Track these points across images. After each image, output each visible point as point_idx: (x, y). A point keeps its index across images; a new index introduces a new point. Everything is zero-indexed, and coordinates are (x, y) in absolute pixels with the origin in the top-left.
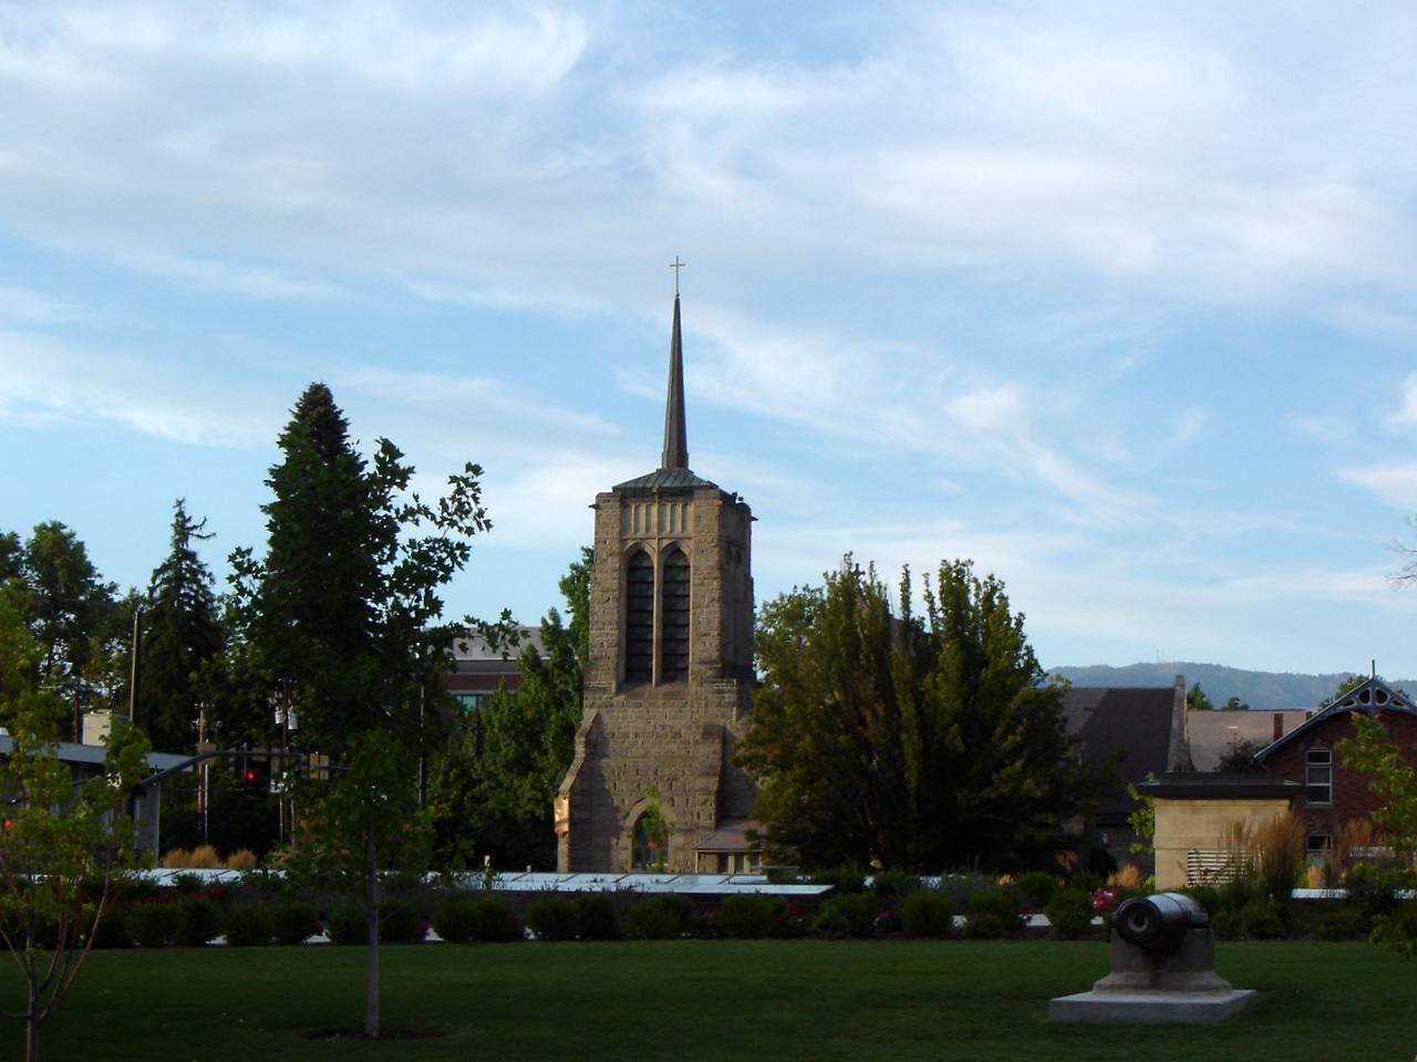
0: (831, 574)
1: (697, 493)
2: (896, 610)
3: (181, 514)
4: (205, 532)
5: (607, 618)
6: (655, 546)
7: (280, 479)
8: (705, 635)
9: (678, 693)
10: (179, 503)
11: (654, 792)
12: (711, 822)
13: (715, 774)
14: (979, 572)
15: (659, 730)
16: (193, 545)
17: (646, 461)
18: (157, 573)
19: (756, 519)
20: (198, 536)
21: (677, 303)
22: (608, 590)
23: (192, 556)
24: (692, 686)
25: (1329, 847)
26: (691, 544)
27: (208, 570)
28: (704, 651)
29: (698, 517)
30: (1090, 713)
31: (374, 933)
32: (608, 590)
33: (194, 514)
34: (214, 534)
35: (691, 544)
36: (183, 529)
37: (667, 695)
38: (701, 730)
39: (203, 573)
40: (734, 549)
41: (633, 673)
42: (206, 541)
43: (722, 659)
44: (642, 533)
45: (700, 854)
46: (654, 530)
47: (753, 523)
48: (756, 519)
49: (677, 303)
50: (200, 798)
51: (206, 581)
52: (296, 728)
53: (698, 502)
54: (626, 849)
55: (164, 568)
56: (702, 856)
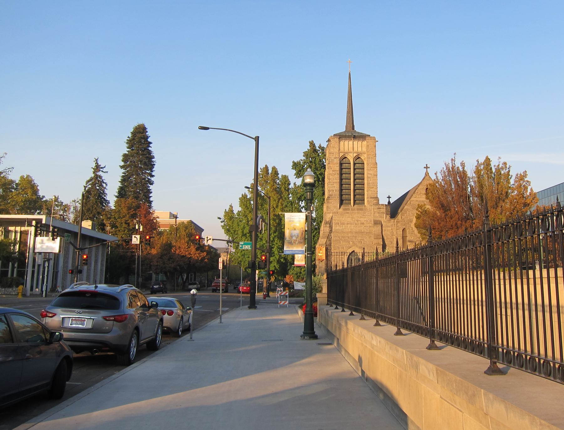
0: (464, 162)
3: (97, 163)
4: (104, 170)
5: (335, 181)
7: (126, 158)
8: (372, 188)
10: (97, 160)
11: (354, 244)
12: (296, 256)
16: (100, 173)
17: (342, 128)
18: (88, 181)
20: (102, 171)
21: (350, 74)
22: (335, 171)
23: (100, 177)
25: (537, 264)
26: (366, 156)
27: (105, 181)
29: (368, 146)
31: (33, 269)
32: (335, 171)
34: (107, 172)
35: (366, 156)
36: (98, 168)
39: (104, 183)
42: (103, 173)
44: (346, 150)
49: (350, 74)
50: (28, 251)
51: (104, 185)
53: (367, 140)
55: (91, 180)
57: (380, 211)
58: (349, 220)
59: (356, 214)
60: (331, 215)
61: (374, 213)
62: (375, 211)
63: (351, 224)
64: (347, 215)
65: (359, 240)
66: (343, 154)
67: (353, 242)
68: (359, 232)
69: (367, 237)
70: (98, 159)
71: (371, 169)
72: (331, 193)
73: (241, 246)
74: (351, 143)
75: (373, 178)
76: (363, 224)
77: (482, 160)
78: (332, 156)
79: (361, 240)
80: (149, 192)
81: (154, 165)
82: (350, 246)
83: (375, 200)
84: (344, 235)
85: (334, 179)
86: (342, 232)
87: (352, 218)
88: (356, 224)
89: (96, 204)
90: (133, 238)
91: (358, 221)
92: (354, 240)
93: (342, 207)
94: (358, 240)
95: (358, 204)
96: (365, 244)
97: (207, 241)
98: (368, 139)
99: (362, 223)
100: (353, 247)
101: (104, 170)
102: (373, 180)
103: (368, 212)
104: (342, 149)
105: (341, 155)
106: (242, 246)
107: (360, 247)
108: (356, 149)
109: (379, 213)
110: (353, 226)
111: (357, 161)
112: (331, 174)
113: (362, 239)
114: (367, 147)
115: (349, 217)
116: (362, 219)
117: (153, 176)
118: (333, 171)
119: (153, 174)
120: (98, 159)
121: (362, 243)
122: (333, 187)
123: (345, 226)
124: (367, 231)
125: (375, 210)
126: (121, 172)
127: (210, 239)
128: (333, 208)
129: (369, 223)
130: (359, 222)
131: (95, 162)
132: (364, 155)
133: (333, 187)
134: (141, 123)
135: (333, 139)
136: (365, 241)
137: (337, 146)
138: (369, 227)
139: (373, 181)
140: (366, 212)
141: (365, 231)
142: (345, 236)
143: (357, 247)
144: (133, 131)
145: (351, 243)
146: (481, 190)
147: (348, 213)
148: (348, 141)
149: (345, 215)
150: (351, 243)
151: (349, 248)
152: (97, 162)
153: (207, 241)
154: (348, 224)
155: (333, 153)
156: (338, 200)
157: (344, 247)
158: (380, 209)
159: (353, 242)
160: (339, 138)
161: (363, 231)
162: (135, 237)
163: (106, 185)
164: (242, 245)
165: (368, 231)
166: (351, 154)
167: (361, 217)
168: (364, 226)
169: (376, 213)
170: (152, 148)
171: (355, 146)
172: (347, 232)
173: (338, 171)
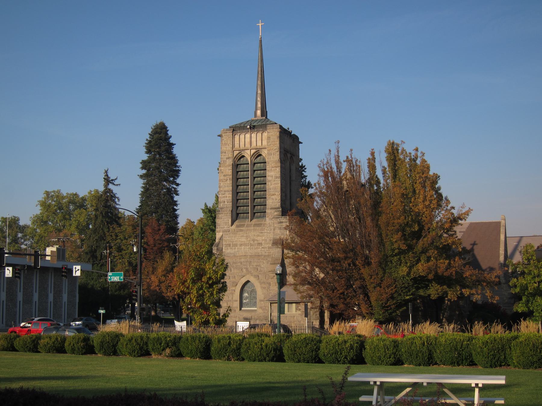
1: (269, 127)
2: (364, 178)
3: (107, 175)
4: (116, 183)
5: (226, 189)
6: (249, 153)
7: (145, 165)
8: (273, 195)
9: (261, 224)
10: (106, 172)
11: (248, 272)
13: (278, 264)
14: (409, 148)
15: (252, 242)
16: (111, 186)
19: (302, 143)
24: (268, 220)
28: (272, 203)
29: (269, 138)
30: (462, 233)
32: (227, 175)
33: (112, 176)
34: (120, 185)
37: (255, 225)
38: (272, 242)
39: (115, 197)
40: (289, 155)
41: (236, 216)
43: (282, 206)
44: (242, 146)
45: (271, 303)
46: (248, 145)
47: (300, 145)
48: (302, 143)
51: (116, 200)
52: (281, 272)
54: (237, 301)
56: (272, 304)
57: (282, 227)
58: (243, 239)
59: (251, 231)
60: (221, 234)
61: (274, 229)
62: (275, 227)
63: (245, 245)
64: (241, 233)
65: (255, 266)
66: (238, 152)
67: (247, 269)
68: (256, 255)
69: (264, 261)
70: (107, 170)
71: (273, 169)
72: (222, 205)
73: (109, 277)
74: (248, 136)
75: (274, 181)
76: (260, 244)
77: (104, 180)
78: (224, 156)
79: (256, 266)
80: (175, 203)
81: (180, 170)
82: (243, 274)
83: (275, 211)
84: (236, 260)
85: (225, 186)
86: (235, 256)
87: (247, 237)
88: (251, 245)
89: (103, 224)
90: (7, 271)
91: (254, 240)
92: (248, 267)
93: (236, 223)
94: (252, 266)
95: (257, 218)
96: (261, 271)
97: (76, 272)
98: (269, 129)
99: (259, 244)
100: (248, 276)
101: (116, 183)
102: (274, 184)
103: (267, 227)
104: (237, 146)
105: (236, 153)
106: (111, 278)
107: (255, 276)
108: (254, 144)
109: (280, 229)
110: (248, 247)
111: (258, 160)
112: (222, 180)
113: (258, 264)
114: (268, 139)
115: (242, 236)
116: (259, 238)
117: (178, 185)
118: (224, 176)
119: (178, 181)
120: (107, 170)
121: (257, 269)
122: (224, 197)
123: (238, 248)
124: (265, 254)
125: (276, 226)
126: (140, 183)
127: (78, 270)
128: (223, 225)
129: (267, 243)
130: (256, 242)
131: (105, 174)
132: (265, 151)
133: (224, 197)
134: (158, 121)
135: (225, 133)
136: (262, 268)
137: (230, 142)
138: (269, 249)
139: (275, 186)
140: (264, 229)
141: (263, 253)
142: (237, 261)
143: (252, 275)
144: (151, 132)
145: (244, 270)
146: (216, 204)
147: (241, 231)
148: (244, 134)
149: (238, 233)
150: (244, 270)
151: (242, 277)
152: (107, 173)
153: (76, 272)
154: (241, 245)
155: (225, 152)
156: (230, 213)
157: (236, 276)
158: (282, 223)
159: (247, 269)
160: (233, 131)
161: (260, 254)
162: (8, 269)
163: (119, 200)
164: (111, 276)
165: (267, 254)
166: (248, 152)
167: (258, 236)
168: (262, 247)
169: (277, 229)
170: (176, 151)
171: (254, 140)
172: (240, 256)
173: (230, 175)
